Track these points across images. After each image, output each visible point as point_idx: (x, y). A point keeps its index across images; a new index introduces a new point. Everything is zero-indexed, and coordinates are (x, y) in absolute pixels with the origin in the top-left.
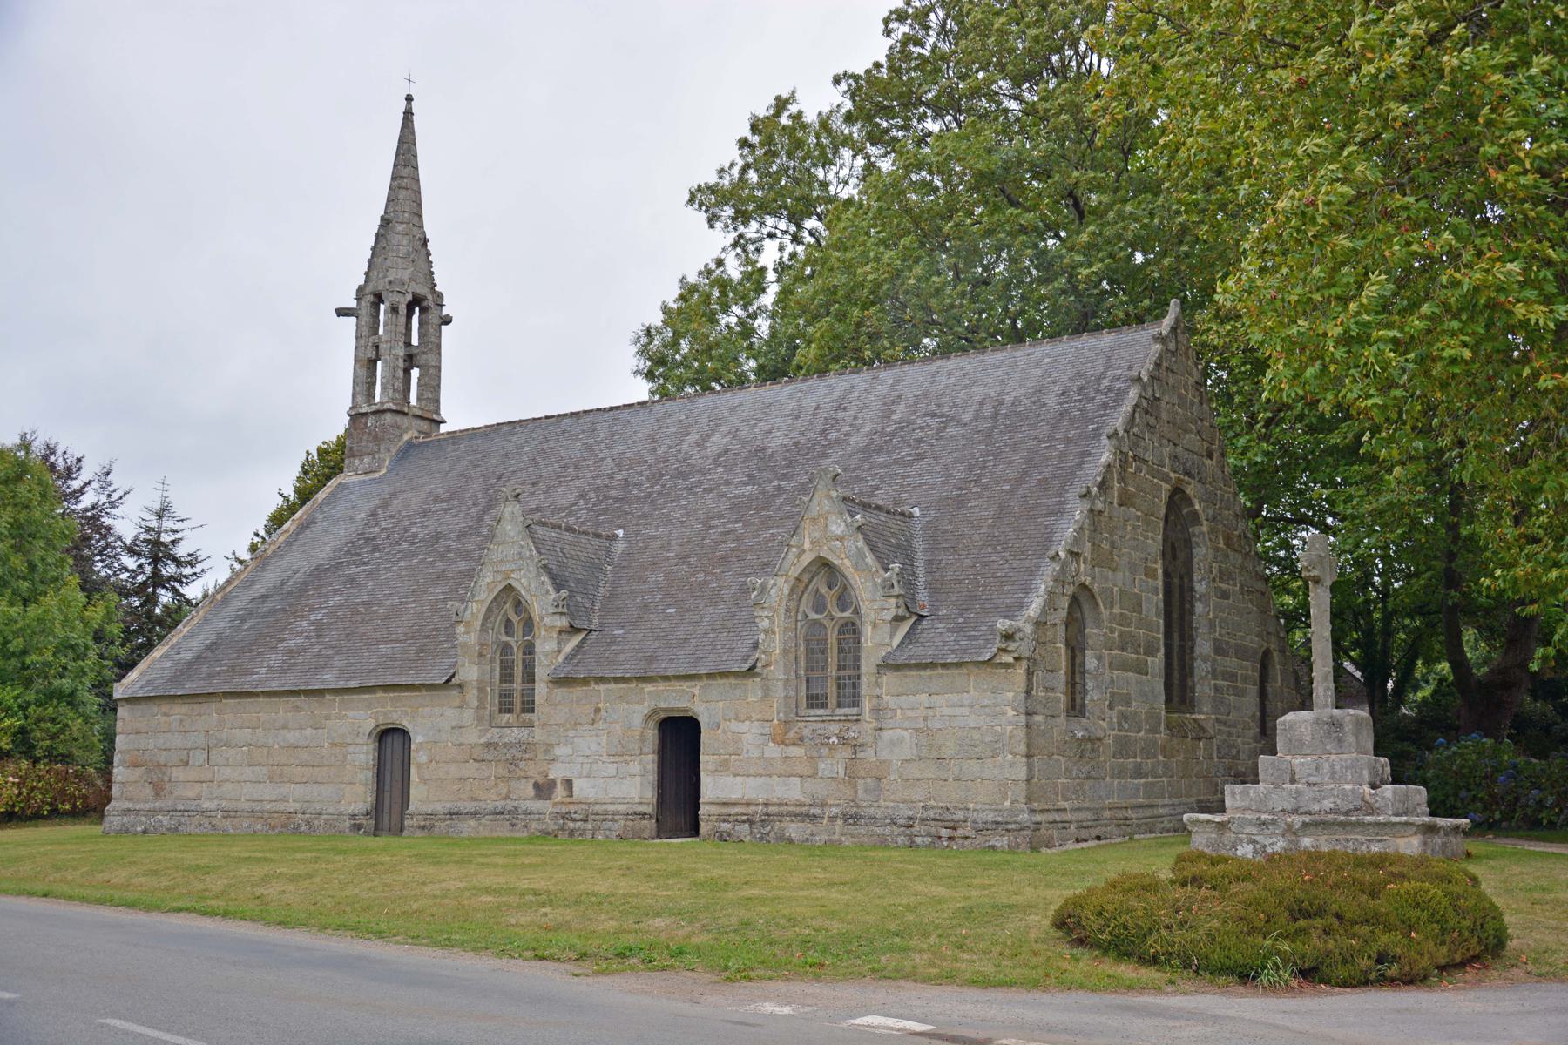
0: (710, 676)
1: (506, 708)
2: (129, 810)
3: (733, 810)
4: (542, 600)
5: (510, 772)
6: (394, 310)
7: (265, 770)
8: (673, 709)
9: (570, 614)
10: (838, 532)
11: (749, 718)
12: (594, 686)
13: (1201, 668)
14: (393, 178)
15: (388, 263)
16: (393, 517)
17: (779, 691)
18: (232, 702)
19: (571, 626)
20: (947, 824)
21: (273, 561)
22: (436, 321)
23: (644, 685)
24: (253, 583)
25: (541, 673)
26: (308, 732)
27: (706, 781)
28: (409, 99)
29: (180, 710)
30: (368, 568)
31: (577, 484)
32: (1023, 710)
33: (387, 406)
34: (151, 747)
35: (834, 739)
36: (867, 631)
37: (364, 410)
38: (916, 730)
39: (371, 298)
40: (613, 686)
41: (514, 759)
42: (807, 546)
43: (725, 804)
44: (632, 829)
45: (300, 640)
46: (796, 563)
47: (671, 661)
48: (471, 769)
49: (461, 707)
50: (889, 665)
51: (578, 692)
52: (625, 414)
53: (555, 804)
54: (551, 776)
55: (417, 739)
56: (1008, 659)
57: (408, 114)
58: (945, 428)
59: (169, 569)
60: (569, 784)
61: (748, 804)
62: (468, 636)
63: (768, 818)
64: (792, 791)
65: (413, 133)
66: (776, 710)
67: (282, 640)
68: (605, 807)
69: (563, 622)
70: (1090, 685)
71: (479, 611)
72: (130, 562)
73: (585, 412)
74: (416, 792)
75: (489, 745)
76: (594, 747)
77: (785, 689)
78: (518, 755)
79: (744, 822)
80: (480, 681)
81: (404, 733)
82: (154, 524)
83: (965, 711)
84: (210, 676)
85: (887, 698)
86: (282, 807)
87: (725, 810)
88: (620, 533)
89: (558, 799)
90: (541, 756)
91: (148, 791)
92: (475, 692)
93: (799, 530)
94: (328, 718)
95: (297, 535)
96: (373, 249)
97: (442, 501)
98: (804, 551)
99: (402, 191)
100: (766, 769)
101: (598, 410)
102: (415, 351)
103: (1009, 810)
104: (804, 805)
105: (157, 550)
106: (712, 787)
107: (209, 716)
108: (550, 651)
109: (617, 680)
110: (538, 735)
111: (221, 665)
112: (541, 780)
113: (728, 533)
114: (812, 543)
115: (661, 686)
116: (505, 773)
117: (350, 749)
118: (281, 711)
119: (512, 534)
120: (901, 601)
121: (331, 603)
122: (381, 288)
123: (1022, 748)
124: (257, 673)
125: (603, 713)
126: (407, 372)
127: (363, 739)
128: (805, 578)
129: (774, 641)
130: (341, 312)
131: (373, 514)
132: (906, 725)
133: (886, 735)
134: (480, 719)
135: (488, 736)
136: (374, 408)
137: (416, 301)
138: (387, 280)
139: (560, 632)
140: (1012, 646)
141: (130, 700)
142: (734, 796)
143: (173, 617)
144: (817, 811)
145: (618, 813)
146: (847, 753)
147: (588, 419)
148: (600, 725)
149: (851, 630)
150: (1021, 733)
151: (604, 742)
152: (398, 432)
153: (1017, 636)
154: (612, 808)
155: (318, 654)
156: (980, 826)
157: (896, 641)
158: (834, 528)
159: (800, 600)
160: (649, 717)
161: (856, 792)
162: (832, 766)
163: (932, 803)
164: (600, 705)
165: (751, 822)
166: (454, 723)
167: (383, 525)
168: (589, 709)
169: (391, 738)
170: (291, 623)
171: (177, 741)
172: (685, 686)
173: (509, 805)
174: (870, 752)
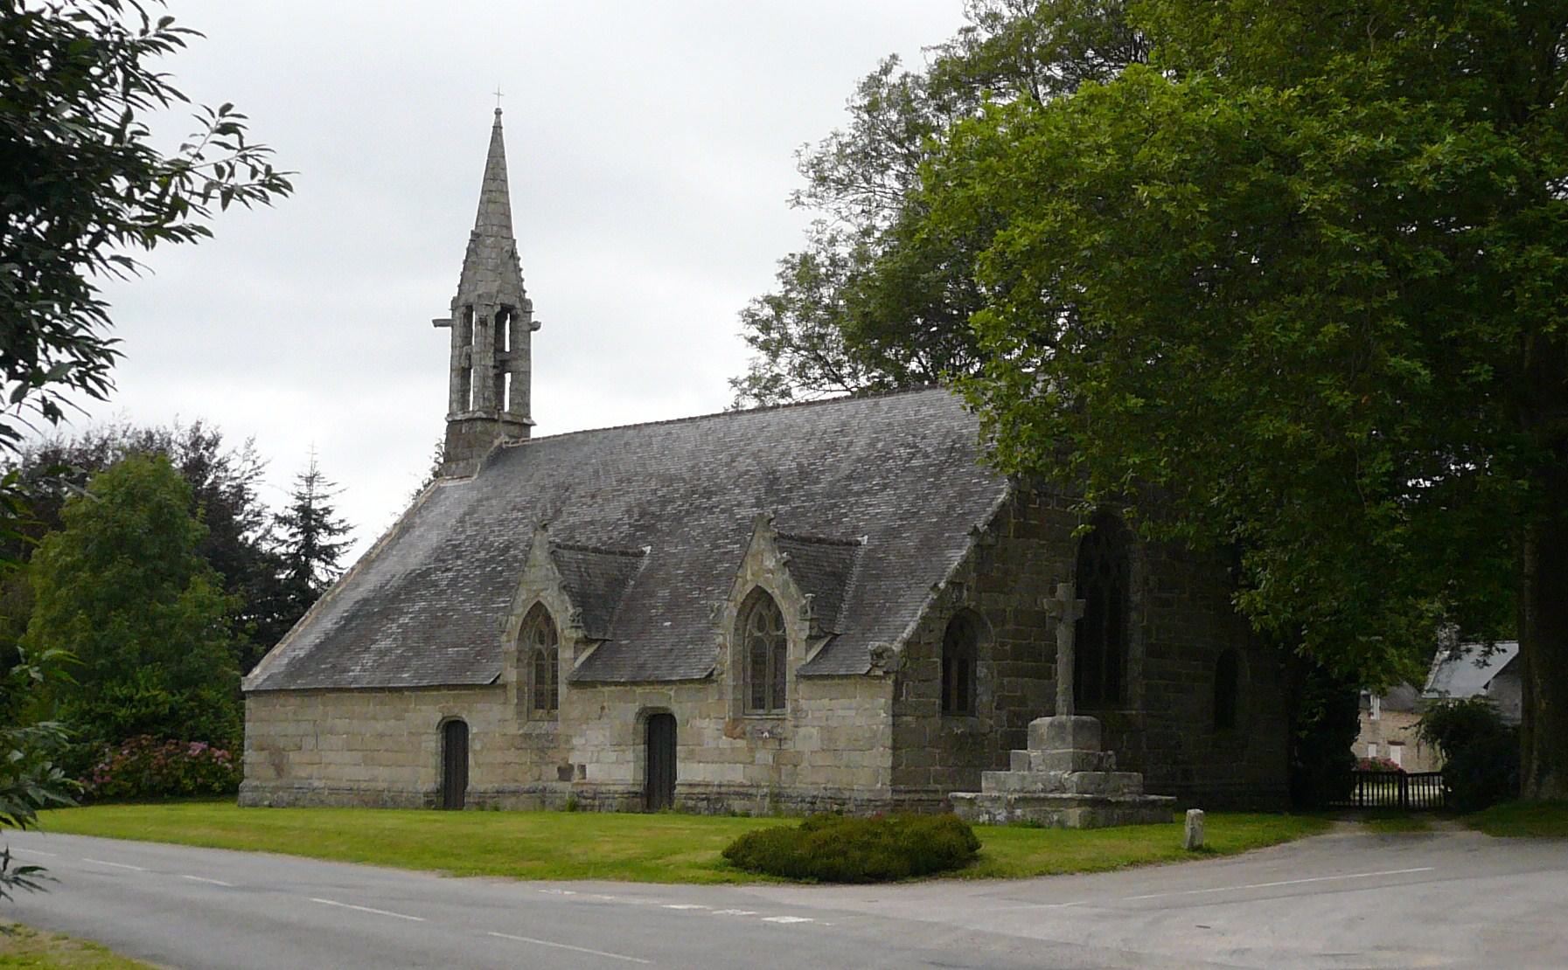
0: (681, 682)
1: (539, 706)
2: (257, 787)
3: (698, 790)
4: (563, 612)
5: (540, 758)
6: (483, 322)
7: (360, 754)
8: (658, 708)
9: (588, 626)
10: (771, 567)
11: (709, 716)
12: (600, 688)
13: (1135, 669)
14: (483, 192)
15: (478, 277)
16: (476, 524)
17: (729, 696)
18: (333, 695)
19: (586, 637)
20: (838, 802)
21: (376, 564)
22: (526, 328)
23: (635, 688)
24: (358, 585)
25: (562, 676)
26: (392, 722)
27: (679, 765)
28: (498, 113)
29: (293, 703)
30: (450, 574)
31: (627, 499)
32: (891, 713)
33: (478, 414)
34: (272, 733)
35: (766, 734)
36: (790, 646)
37: (458, 418)
38: (821, 727)
39: (463, 309)
40: (613, 688)
41: (543, 746)
42: (749, 577)
43: (690, 785)
44: (627, 804)
45: (389, 641)
46: (742, 591)
47: (657, 668)
48: (511, 755)
49: (505, 703)
50: (803, 677)
51: (589, 692)
52: (675, 429)
53: (574, 785)
54: (570, 762)
55: (473, 730)
56: (880, 673)
57: (497, 128)
58: (911, 459)
59: (323, 539)
60: (583, 768)
61: (707, 785)
62: (509, 644)
63: (720, 797)
64: (736, 775)
65: (502, 147)
66: (728, 714)
67: (375, 642)
68: (608, 787)
69: (580, 634)
70: (980, 690)
71: (517, 623)
72: (282, 532)
73: (647, 424)
74: (474, 775)
75: (527, 736)
76: (601, 738)
77: (733, 693)
78: (546, 744)
79: (703, 800)
80: (519, 682)
81: (465, 725)
82: (304, 490)
83: (853, 713)
84: (318, 672)
85: (802, 701)
86: (372, 785)
87: (691, 791)
88: (648, 549)
89: (575, 782)
90: (563, 746)
91: (271, 772)
92: (515, 691)
93: (744, 564)
94: (406, 711)
95: (399, 539)
96: (465, 262)
97: (519, 510)
98: (747, 581)
99: (490, 205)
100: (720, 757)
101: (657, 423)
102: (508, 358)
103: (879, 791)
104: (744, 786)
105: (309, 519)
106: (688, 772)
107: (317, 710)
108: (570, 659)
109: (617, 684)
110: (561, 728)
111: (326, 663)
112: (562, 764)
113: (726, 553)
114: (753, 575)
115: (648, 689)
116: (536, 758)
117: (424, 737)
118: (370, 706)
119: (540, 558)
120: (815, 624)
121: (417, 608)
122: (472, 300)
123: (889, 742)
124: (353, 671)
125: (607, 710)
126: (500, 378)
127: (432, 730)
128: (750, 602)
129: (725, 653)
130: (437, 323)
131: (462, 521)
132: (815, 724)
133: (802, 731)
134: (519, 713)
135: (525, 728)
136: (467, 416)
137: (506, 310)
138: (477, 293)
139: (577, 642)
140: (882, 663)
141: (256, 693)
142: (698, 779)
143: (309, 598)
144: (753, 791)
145: (616, 792)
146: (774, 745)
147: (648, 431)
148: (605, 720)
149: (782, 644)
150: (889, 731)
151: (608, 734)
152: (487, 438)
153: (885, 655)
154: (612, 788)
155: (401, 656)
156: (859, 803)
157: (809, 658)
158: (767, 563)
159: (747, 620)
160: (639, 714)
161: (780, 776)
162: (764, 756)
163: (829, 785)
164: (605, 704)
165: (708, 799)
166: (499, 717)
167: (468, 533)
168: (597, 708)
169: (454, 734)
170: (384, 626)
171: (291, 729)
172: (665, 689)
173: (540, 785)
174: (790, 744)
